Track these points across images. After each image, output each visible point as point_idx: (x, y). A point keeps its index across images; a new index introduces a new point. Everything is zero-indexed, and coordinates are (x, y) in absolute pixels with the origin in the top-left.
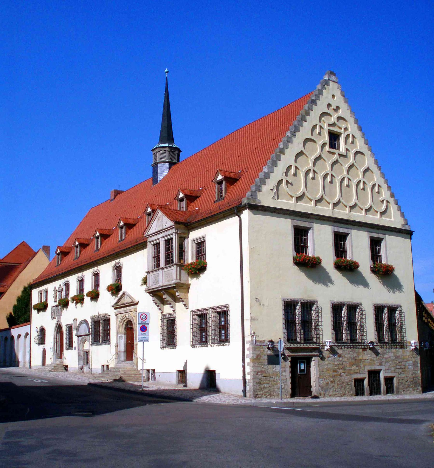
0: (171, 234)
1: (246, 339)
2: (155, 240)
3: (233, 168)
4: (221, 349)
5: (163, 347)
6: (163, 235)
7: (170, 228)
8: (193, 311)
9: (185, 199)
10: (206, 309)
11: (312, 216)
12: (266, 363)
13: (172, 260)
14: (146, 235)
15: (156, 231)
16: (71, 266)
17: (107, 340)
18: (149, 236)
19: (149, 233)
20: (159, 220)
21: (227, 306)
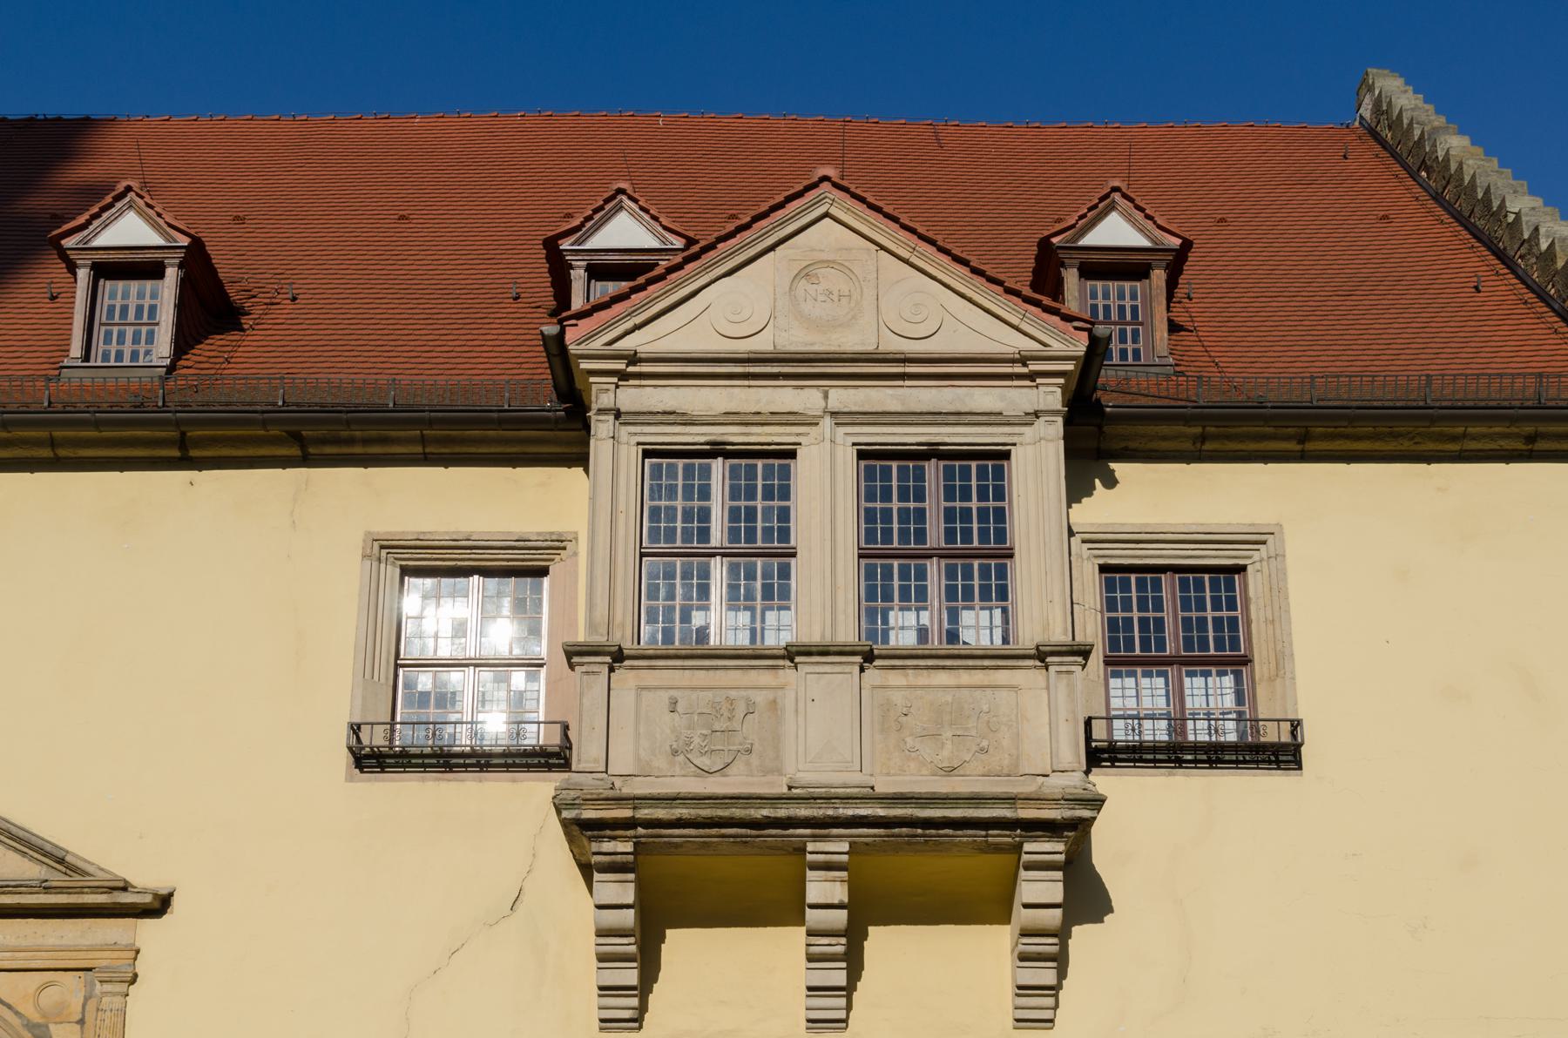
0: (992, 418)
14: (597, 345)
15: (762, 344)
18: (632, 368)
20: (805, 273)
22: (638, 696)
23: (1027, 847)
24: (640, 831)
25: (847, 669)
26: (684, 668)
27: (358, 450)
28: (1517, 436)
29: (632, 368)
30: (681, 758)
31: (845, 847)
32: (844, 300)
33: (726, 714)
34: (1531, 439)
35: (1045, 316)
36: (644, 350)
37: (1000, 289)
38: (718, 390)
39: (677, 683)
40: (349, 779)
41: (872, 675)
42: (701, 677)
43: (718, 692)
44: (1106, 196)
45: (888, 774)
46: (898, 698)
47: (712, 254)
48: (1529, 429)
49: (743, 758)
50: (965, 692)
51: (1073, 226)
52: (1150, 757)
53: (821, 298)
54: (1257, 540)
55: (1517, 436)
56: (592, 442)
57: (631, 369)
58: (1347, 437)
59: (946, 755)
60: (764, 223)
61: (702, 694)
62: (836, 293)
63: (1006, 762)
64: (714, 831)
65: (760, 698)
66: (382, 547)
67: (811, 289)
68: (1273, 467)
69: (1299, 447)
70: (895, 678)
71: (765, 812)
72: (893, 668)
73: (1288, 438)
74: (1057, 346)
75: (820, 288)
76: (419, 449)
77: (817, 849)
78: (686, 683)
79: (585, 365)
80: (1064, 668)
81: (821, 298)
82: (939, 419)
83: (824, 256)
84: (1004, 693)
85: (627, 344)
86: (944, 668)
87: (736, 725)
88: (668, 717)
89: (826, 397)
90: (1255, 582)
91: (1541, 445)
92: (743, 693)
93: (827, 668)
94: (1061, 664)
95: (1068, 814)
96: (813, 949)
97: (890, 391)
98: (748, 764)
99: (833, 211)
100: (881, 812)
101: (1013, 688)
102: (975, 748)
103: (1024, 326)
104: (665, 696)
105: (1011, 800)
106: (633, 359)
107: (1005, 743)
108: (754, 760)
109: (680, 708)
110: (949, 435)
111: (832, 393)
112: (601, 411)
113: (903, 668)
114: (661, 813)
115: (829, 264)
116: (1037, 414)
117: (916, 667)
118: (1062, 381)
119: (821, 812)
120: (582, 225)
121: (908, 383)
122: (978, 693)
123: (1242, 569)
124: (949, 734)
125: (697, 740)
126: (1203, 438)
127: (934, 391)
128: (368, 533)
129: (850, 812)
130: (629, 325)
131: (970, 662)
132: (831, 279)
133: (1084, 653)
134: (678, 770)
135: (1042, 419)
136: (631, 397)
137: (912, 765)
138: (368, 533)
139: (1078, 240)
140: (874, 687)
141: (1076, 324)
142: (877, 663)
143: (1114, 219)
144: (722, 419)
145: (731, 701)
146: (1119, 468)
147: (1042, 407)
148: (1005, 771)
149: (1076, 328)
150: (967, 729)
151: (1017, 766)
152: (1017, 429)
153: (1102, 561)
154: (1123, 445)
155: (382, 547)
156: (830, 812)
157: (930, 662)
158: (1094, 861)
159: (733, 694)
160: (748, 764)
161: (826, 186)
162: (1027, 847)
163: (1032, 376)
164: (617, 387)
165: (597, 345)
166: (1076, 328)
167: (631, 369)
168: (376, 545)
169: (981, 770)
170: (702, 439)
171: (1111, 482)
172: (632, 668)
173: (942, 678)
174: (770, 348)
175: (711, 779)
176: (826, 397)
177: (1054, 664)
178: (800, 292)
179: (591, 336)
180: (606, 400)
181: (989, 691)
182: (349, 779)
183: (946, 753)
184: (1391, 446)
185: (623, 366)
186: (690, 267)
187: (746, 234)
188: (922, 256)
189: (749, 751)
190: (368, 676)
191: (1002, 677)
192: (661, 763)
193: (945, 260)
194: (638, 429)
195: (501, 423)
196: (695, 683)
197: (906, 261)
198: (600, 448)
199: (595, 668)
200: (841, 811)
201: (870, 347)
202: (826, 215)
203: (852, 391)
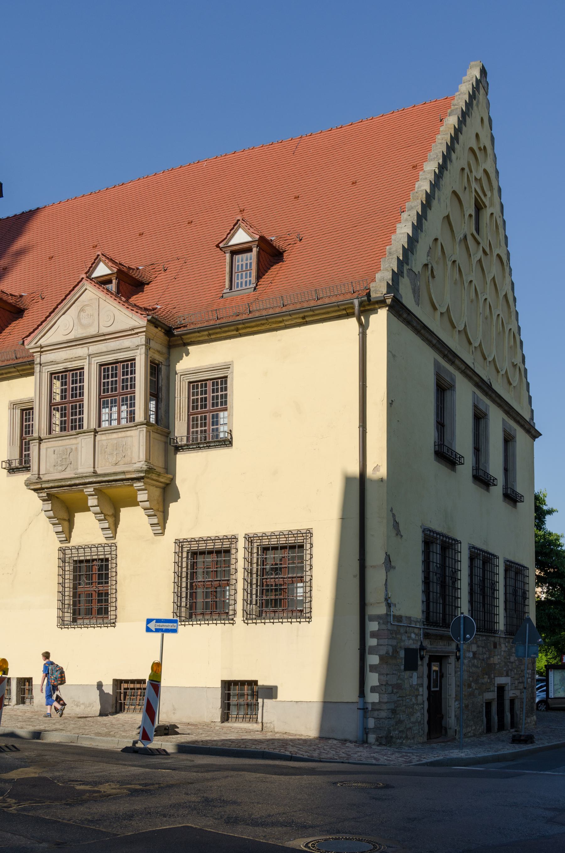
0: (128, 349)
1: (371, 611)
2: (66, 361)
3: (135, 261)
4: (277, 633)
5: (62, 624)
6: (94, 348)
7: (131, 332)
8: (179, 543)
9: (255, 250)
10: (234, 539)
11: (457, 362)
12: (402, 667)
13: (81, 420)
14: (32, 345)
15: (71, 337)
16: (253, 308)
17: (299, 611)
18: (42, 350)
19: (43, 342)
20: (82, 310)
21: (309, 533)
22: (46, 450)
23: (135, 485)
24: (46, 490)
27: (5, 376)
28: (299, 318)
29: (42, 350)
31: (92, 489)
34: (304, 318)
36: (43, 344)
40: (8, 476)
42: (60, 443)
44: (237, 223)
46: (104, 443)
47: (57, 309)
48: (302, 315)
50: (120, 439)
51: (226, 238)
52: (191, 447)
54: (227, 367)
55: (299, 318)
57: (42, 350)
58: (249, 327)
59: (114, 459)
60: (69, 296)
64: (61, 488)
65: (73, 447)
68: (232, 340)
69: (238, 333)
72: (103, 434)
73: (233, 331)
75: (86, 314)
76: (18, 373)
78: (56, 445)
79: (31, 351)
82: (115, 352)
83: (86, 303)
90: (229, 380)
91: (308, 319)
93: (86, 437)
94: (140, 428)
97: (103, 345)
100: (95, 480)
101: (131, 436)
104: (52, 449)
105: (124, 473)
106: (41, 347)
107: (129, 454)
111: (90, 348)
113: (105, 434)
117: (108, 433)
118: (144, 334)
120: (89, 270)
121: (108, 341)
123: (226, 377)
125: (59, 462)
126: (210, 335)
128: (10, 401)
130: (40, 336)
131: (120, 430)
132: (88, 310)
133: (50, 433)
136: (46, 358)
138: (10, 401)
139: (228, 243)
142: (99, 433)
143: (241, 231)
145: (66, 449)
146: (190, 348)
151: (131, 461)
152: (136, 351)
153: (188, 381)
154: (190, 340)
157: (111, 431)
162: (135, 485)
163: (137, 333)
165: (32, 345)
167: (42, 350)
169: (123, 463)
170: (62, 368)
171: (188, 354)
173: (115, 436)
174: (73, 337)
176: (88, 349)
178: (81, 316)
179: (31, 342)
182: (8, 476)
184: (263, 328)
186: (52, 315)
187: (65, 301)
191: (129, 433)
192: (52, 470)
203: (95, 346)
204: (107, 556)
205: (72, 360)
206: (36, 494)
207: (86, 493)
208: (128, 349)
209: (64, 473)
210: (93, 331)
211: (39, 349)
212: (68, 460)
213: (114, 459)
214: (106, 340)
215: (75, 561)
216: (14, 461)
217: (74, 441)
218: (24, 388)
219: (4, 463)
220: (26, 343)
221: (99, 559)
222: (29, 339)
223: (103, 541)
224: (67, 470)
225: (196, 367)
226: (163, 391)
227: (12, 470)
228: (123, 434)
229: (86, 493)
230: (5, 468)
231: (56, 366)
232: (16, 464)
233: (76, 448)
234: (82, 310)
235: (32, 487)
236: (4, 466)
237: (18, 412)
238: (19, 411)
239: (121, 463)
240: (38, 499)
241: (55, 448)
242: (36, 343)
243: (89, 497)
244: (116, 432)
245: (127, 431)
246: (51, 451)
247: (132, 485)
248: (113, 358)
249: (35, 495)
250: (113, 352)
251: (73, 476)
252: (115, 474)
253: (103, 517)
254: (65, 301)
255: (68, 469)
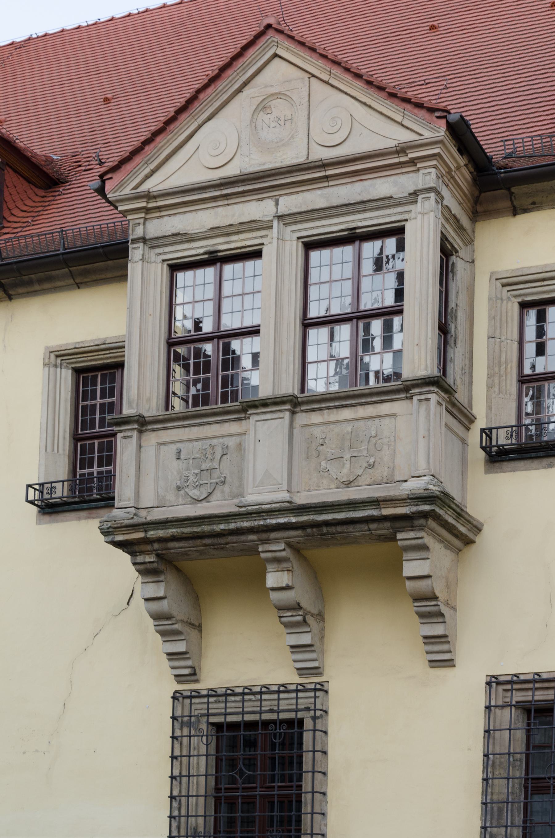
2: (216, 232)
6: (290, 203)
7: (400, 159)
14: (127, 191)
18: (154, 204)
20: (263, 107)
22: (158, 450)
23: (399, 536)
25: (281, 415)
26: (184, 427)
29: (154, 204)
30: (182, 492)
32: (288, 123)
33: (210, 457)
35: (416, 111)
37: (384, 94)
38: (208, 211)
39: (181, 438)
41: (302, 418)
42: (195, 432)
43: (205, 441)
45: (309, 490)
46: (317, 432)
49: (220, 488)
50: (361, 423)
53: (273, 125)
56: (130, 265)
59: (345, 473)
61: (195, 444)
62: (282, 118)
63: (385, 473)
65: (231, 442)
66: (57, 356)
67: (266, 118)
70: (316, 418)
71: (222, 527)
72: (314, 410)
74: (427, 134)
75: (272, 116)
77: (268, 550)
78: (186, 437)
80: (423, 397)
81: (273, 125)
82: (351, 208)
84: (387, 421)
85: (144, 187)
86: (346, 406)
87: (215, 464)
88: (175, 463)
89: (277, 204)
92: (221, 440)
93: (268, 416)
94: (420, 394)
95: (414, 509)
96: (283, 619)
97: (319, 192)
98: (223, 492)
99: (280, 52)
100: (293, 520)
101: (393, 416)
102: (365, 465)
103: (406, 123)
105: (376, 502)
106: (149, 196)
107: (386, 459)
108: (226, 488)
109: (182, 457)
110: (361, 220)
111: (282, 200)
112: (135, 241)
113: (321, 409)
114: (161, 533)
115: (277, 95)
116: (415, 194)
117: (329, 408)
119: (256, 523)
122: (370, 422)
124: (348, 456)
125: (192, 478)
127: (349, 186)
129: (274, 521)
132: (280, 108)
133: (167, 409)
134: (181, 501)
135: (420, 197)
136: (159, 226)
137: (325, 482)
138: (47, 348)
140: (303, 426)
141: (437, 114)
144: (210, 233)
145: (212, 447)
147: (420, 187)
148: (385, 481)
149: (438, 117)
150: (360, 451)
152: (406, 208)
153: (520, 300)
155: (57, 356)
156: (262, 523)
158: (127, 555)
159: (215, 441)
160: (223, 492)
161: (271, 33)
162: (399, 536)
163: (413, 162)
164: (145, 219)
166: (438, 117)
167: (151, 205)
168: (52, 356)
169: (369, 481)
170: (201, 251)
172: (154, 430)
173: (347, 414)
174: (237, 172)
175: (200, 505)
176: (277, 204)
177: (416, 394)
178: (259, 122)
179: (121, 185)
180: (139, 232)
181: (377, 420)
183: (345, 471)
185: (144, 204)
188: (336, 77)
189: (223, 483)
190: (49, 449)
191: (385, 408)
192: (171, 497)
193: (348, 77)
194: (299, 226)
195: (390, 206)
196: (191, 437)
197: (327, 83)
198: (134, 269)
199: (129, 434)
200: (268, 521)
201: (301, 159)
202: (276, 55)
203: (294, 196)
204: (300, 715)
205: (232, 229)
206: (127, 557)
207: (263, 555)
208: (387, 202)
209: (204, 504)
210: (293, 155)
211: (142, 204)
212: (216, 474)
213: (345, 471)
214: (327, 178)
215: (218, 727)
216: (59, 486)
217: (233, 428)
218: (84, 318)
219: (31, 491)
220: (109, 186)
221: (282, 721)
222: (117, 177)
223: (291, 678)
224: (214, 497)
225: (546, 266)
226: (459, 319)
227: (49, 508)
228: (370, 410)
229: (263, 555)
230: (32, 502)
231: (186, 246)
232: (61, 491)
233: (240, 446)
234: (263, 107)
235: (119, 538)
236: (31, 498)
237: (67, 375)
238: (70, 372)
239: (361, 481)
240: (133, 568)
241: (179, 445)
242: (136, 188)
243: (269, 567)
244: (351, 406)
245: (382, 402)
246: (170, 451)
247: (393, 539)
248: (343, 227)
249: (123, 558)
250: (344, 209)
251: (235, 509)
252: (352, 505)
253: (300, 618)
254: (221, 85)
255: (217, 495)
